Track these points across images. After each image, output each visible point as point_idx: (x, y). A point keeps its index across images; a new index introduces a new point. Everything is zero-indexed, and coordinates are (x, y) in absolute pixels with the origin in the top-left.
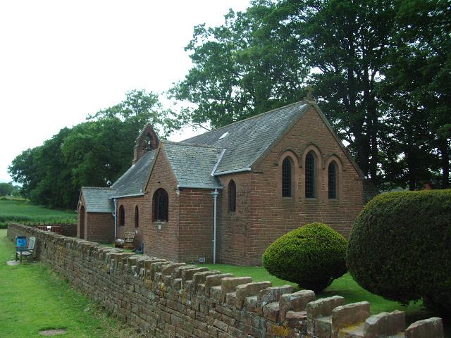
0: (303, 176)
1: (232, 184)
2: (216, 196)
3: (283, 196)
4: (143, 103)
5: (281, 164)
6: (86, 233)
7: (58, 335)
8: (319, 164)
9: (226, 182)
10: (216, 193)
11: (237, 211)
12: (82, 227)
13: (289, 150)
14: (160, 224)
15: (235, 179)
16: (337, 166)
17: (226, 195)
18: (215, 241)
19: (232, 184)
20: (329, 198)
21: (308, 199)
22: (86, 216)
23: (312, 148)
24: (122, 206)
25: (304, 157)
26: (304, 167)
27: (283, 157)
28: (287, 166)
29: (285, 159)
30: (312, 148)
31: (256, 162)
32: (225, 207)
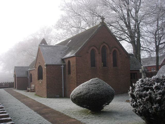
0: (101, 57)
1: (69, 62)
2: (63, 68)
3: (91, 67)
4: (49, 30)
5: (90, 52)
6: (17, 87)
7: (73, 122)
8: (108, 51)
9: (67, 61)
10: (63, 66)
11: (71, 74)
12: (15, 83)
13: (93, 46)
14: (40, 81)
15: (70, 60)
16: (117, 52)
17: (67, 67)
18: (63, 87)
19: (69, 62)
20: (114, 66)
21: (92, 67)
22: (16, 78)
23: (105, 44)
24: (31, 74)
25: (101, 49)
26: (101, 53)
27: (91, 49)
28: (93, 52)
29: (114, 51)
30: (105, 44)
31: (78, 52)
32: (67, 73)
